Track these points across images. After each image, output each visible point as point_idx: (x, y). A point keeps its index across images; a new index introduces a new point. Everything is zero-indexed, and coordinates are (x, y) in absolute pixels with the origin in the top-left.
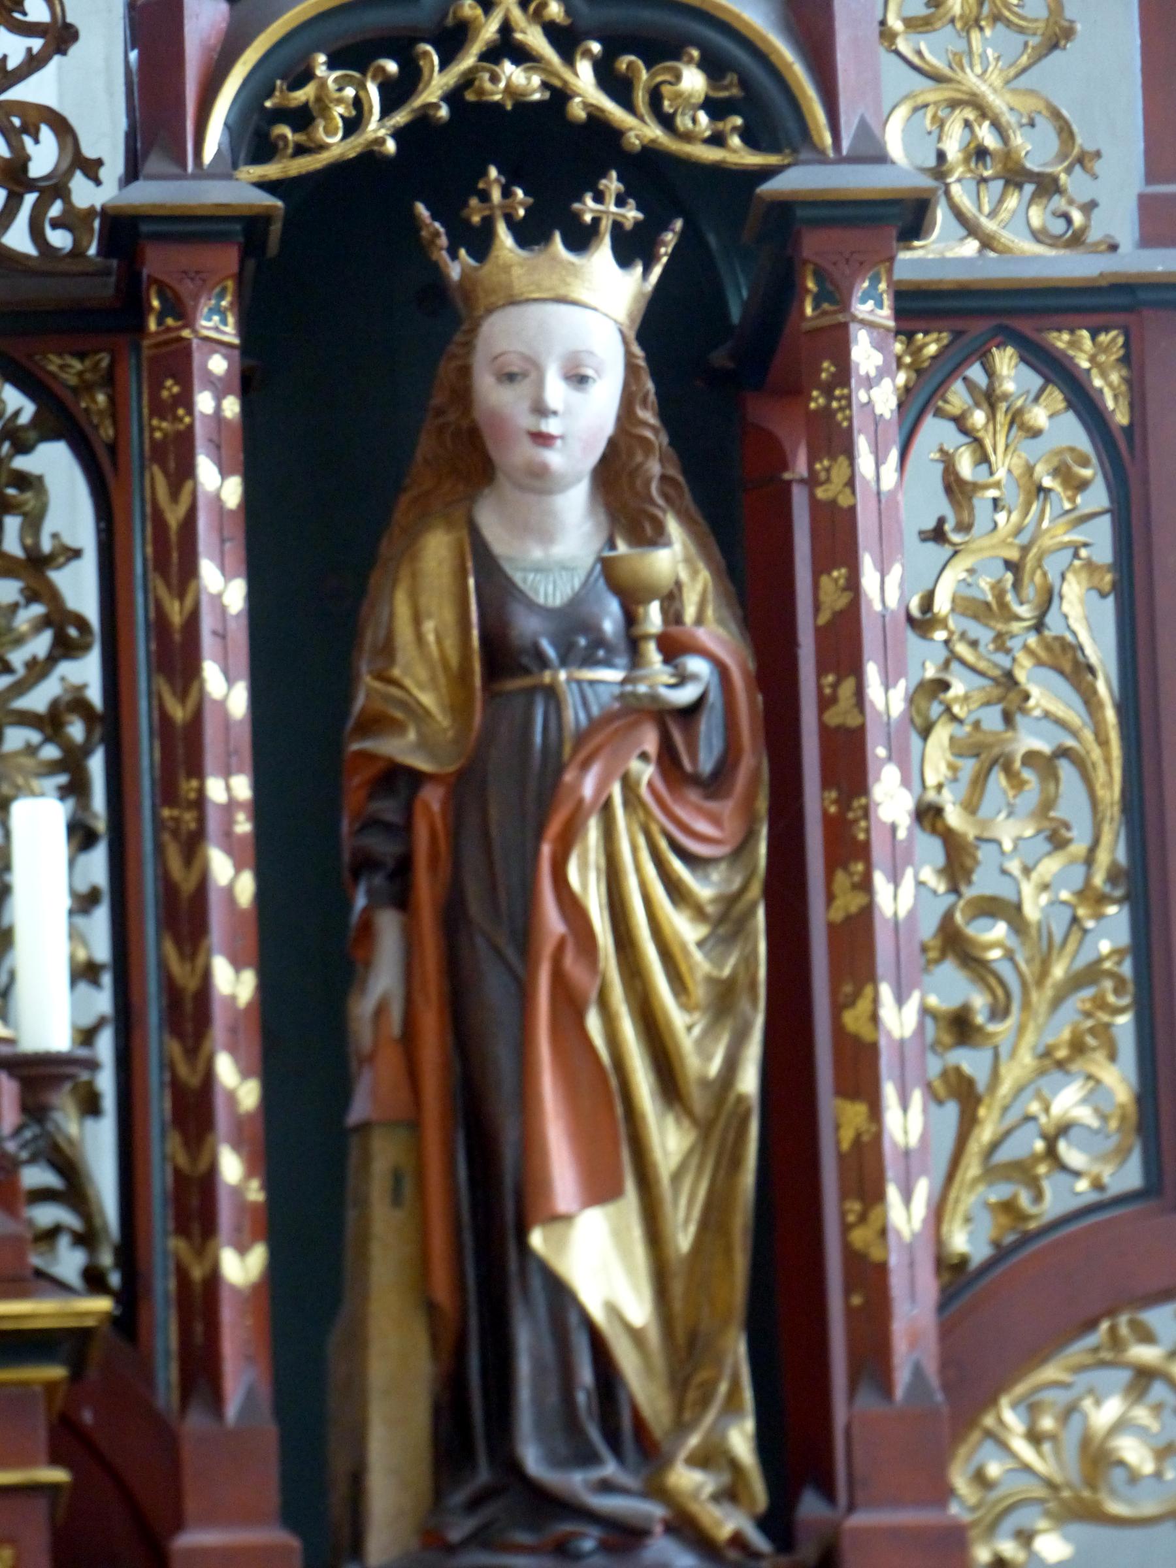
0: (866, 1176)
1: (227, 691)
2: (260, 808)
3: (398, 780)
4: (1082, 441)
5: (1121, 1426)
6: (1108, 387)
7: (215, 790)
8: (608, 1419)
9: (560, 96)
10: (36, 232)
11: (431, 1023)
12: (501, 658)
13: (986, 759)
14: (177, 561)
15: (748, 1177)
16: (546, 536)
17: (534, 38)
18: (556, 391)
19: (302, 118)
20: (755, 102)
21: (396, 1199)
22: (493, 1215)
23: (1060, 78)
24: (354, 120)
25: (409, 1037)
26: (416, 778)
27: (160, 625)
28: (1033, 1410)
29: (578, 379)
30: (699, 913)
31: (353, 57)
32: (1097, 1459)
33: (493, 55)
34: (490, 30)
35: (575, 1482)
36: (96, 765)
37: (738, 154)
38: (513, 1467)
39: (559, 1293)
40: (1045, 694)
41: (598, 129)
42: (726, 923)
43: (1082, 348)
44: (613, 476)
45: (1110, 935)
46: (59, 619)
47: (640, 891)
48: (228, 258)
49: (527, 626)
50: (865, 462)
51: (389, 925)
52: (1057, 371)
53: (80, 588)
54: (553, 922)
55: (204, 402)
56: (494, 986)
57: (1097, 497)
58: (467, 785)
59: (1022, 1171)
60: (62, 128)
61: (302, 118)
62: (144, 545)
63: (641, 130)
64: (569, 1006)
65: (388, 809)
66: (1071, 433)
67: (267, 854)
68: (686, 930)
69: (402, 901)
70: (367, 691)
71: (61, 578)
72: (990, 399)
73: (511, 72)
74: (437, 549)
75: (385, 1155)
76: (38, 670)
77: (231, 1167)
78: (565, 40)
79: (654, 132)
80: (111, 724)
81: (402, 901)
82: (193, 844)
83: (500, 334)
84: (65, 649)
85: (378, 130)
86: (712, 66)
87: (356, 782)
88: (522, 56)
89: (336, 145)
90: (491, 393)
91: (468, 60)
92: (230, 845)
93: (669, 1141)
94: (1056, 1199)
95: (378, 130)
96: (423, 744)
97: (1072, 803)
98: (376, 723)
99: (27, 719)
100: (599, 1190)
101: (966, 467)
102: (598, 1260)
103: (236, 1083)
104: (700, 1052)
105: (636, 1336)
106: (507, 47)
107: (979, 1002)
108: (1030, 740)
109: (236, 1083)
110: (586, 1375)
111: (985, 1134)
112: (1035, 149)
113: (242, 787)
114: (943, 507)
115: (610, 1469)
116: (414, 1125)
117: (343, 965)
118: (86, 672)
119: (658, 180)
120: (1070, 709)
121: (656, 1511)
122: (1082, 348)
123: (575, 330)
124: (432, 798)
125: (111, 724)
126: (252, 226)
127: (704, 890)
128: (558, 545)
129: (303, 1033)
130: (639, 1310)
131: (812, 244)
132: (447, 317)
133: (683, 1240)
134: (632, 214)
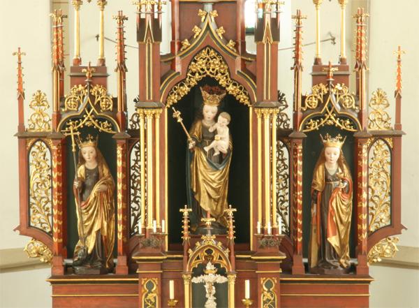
0: (361, 232)
1: (300, 173)
2: (303, 195)
3: (315, 191)
4: (388, 149)
5: (387, 249)
6: (390, 143)
7: (299, 193)
8: (336, 256)
9: (335, 123)
10: (284, 126)
11: (319, 216)
12: (327, 179)
13: (377, 182)
14: (296, 160)
15: (349, 230)
16: (332, 167)
17: (332, 118)
18: (333, 155)
19: (310, 126)
20: (353, 124)
21: (315, 232)
22: (324, 236)
23: (387, 110)
24: (314, 126)
25: (316, 216)
26: (318, 192)
27: (294, 222)
28: (378, 246)
29: (335, 154)
30: (345, 206)
31: (314, 119)
32: (384, 252)
33: (328, 119)
34: (328, 117)
35: (331, 261)
36: (288, 180)
37: (352, 130)
38: (325, 259)
39: (330, 244)
40: (383, 175)
41: (339, 127)
42: (348, 206)
43: (388, 140)
44: (339, 162)
45: (388, 199)
46: (285, 165)
47: (340, 205)
48: (301, 141)
49: (329, 177)
50: (363, 162)
51: (315, 205)
52: (386, 142)
53: (287, 162)
54: (330, 209)
55: (299, 155)
56: (325, 215)
57: (389, 154)
58: (323, 192)
59: (378, 223)
60: (287, 116)
61: (310, 126)
62: (293, 159)
63: (343, 127)
64: (332, 217)
65: (315, 194)
66: (387, 148)
67: (303, 199)
68: (343, 207)
69: (316, 203)
70: (314, 181)
71: (285, 161)
72: (378, 144)
73: (330, 121)
74: (321, 167)
75: (314, 228)
76: (283, 170)
77: (299, 230)
78: (336, 118)
79: (344, 127)
80: (289, 176)
81: (316, 203)
82: (296, 199)
83: (327, 150)
84: (285, 169)
85: (317, 127)
86: (350, 121)
87: (312, 191)
88: (331, 119)
89: (312, 128)
90: (327, 155)
91: (326, 120)
92: (300, 198)
93: (341, 228)
94: (382, 225)
95: (317, 127)
96: (319, 188)
97: (385, 186)
98: (314, 185)
99: (282, 175)
100: (334, 234)
101: (376, 152)
102: (334, 241)
103: (300, 222)
104: (345, 219)
105: (338, 247)
106: (330, 119)
107: (374, 206)
108: (381, 180)
109: (300, 222)
110: (332, 251)
111: (374, 219)
112: (385, 118)
113: (301, 192)
114: (373, 156)
115: (335, 260)
116: (317, 225)
117: (311, 207)
118: (287, 171)
119: (344, 133)
120: (385, 176)
121: (338, 264)
122: (388, 140)
123: (335, 148)
124: (320, 194)
125: (289, 176)
126: (304, 139)
127: (345, 203)
128: (333, 168)
129: (307, 217)
130: (338, 245)
131: (359, 140)
132: (323, 146)
133: (343, 237)
134: (341, 138)
